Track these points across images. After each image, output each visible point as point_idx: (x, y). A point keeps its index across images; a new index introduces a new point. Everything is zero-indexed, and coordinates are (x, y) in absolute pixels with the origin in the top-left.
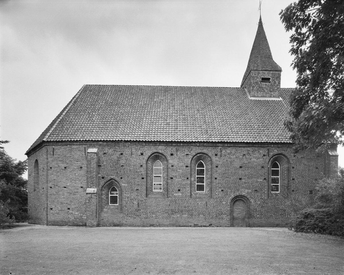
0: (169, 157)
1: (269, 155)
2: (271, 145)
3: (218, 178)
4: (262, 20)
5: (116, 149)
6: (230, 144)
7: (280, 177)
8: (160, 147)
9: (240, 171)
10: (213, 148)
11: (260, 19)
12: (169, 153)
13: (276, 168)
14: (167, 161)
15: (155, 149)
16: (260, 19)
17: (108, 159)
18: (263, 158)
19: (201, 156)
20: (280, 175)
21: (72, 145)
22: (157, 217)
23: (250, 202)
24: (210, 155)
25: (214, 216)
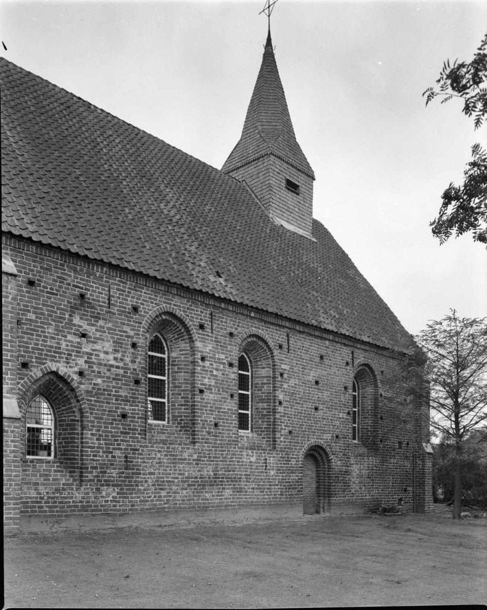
0: (196, 334)
1: (353, 363)
2: (250, 311)
3: (285, 404)
4: (273, 43)
5: (66, 274)
6: (233, 306)
7: (359, 410)
8: (177, 300)
9: (316, 394)
10: (276, 330)
11: (269, 39)
12: (197, 322)
13: (244, 371)
14: (191, 340)
15: (167, 303)
16: (269, 39)
17: (43, 305)
18: (347, 369)
19: (253, 342)
20: (359, 406)
21: (338, 342)
22: (171, 496)
23: (82, 443)
24: (271, 344)
25: (278, 491)
